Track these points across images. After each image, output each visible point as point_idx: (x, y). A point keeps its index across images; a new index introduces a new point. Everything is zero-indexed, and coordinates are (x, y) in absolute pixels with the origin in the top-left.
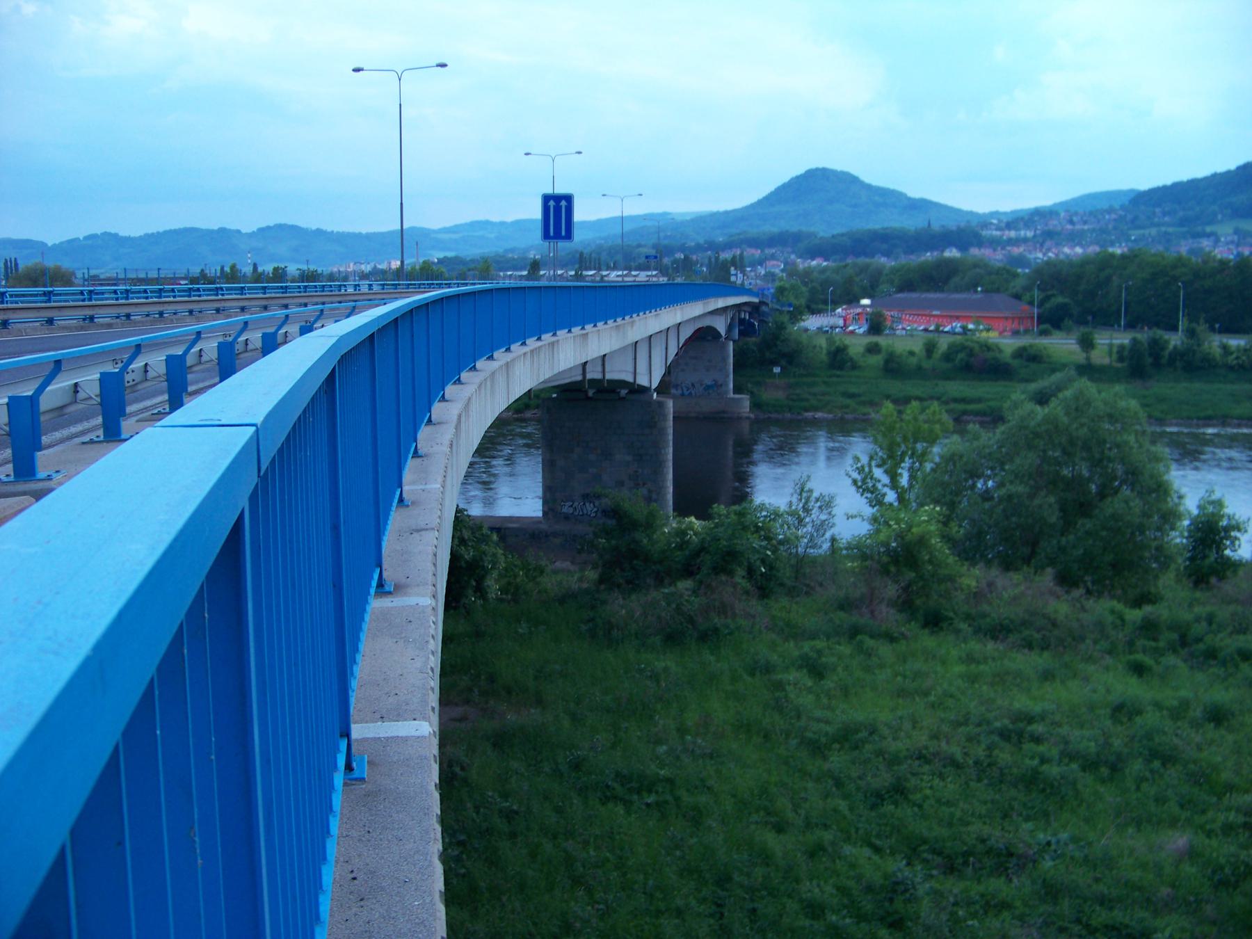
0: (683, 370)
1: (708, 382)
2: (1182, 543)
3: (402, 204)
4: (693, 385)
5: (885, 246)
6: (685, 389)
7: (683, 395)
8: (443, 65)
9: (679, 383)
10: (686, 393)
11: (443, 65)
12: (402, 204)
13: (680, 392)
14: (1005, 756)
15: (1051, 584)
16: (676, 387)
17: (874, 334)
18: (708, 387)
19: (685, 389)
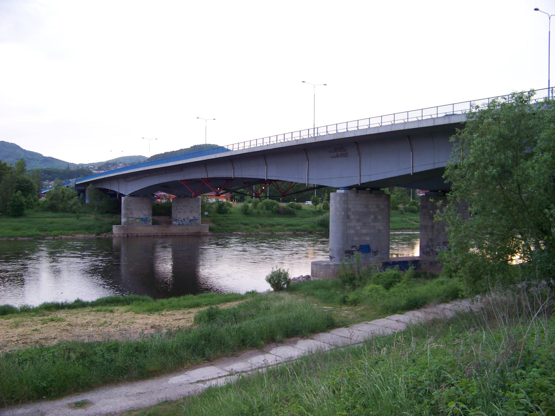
0: (179, 212)
1: (191, 218)
2: (552, 279)
3: (549, 80)
4: (184, 219)
5: (50, 176)
6: (180, 222)
7: (179, 224)
8: (215, 119)
9: (177, 218)
10: (181, 223)
11: (215, 119)
12: (549, 80)
13: (178, 223)
14: (332, 297)
15: (371, 253)
16: (176, 220)
17: (323, 220)
18: (191, 220)
19: (180, 222)
